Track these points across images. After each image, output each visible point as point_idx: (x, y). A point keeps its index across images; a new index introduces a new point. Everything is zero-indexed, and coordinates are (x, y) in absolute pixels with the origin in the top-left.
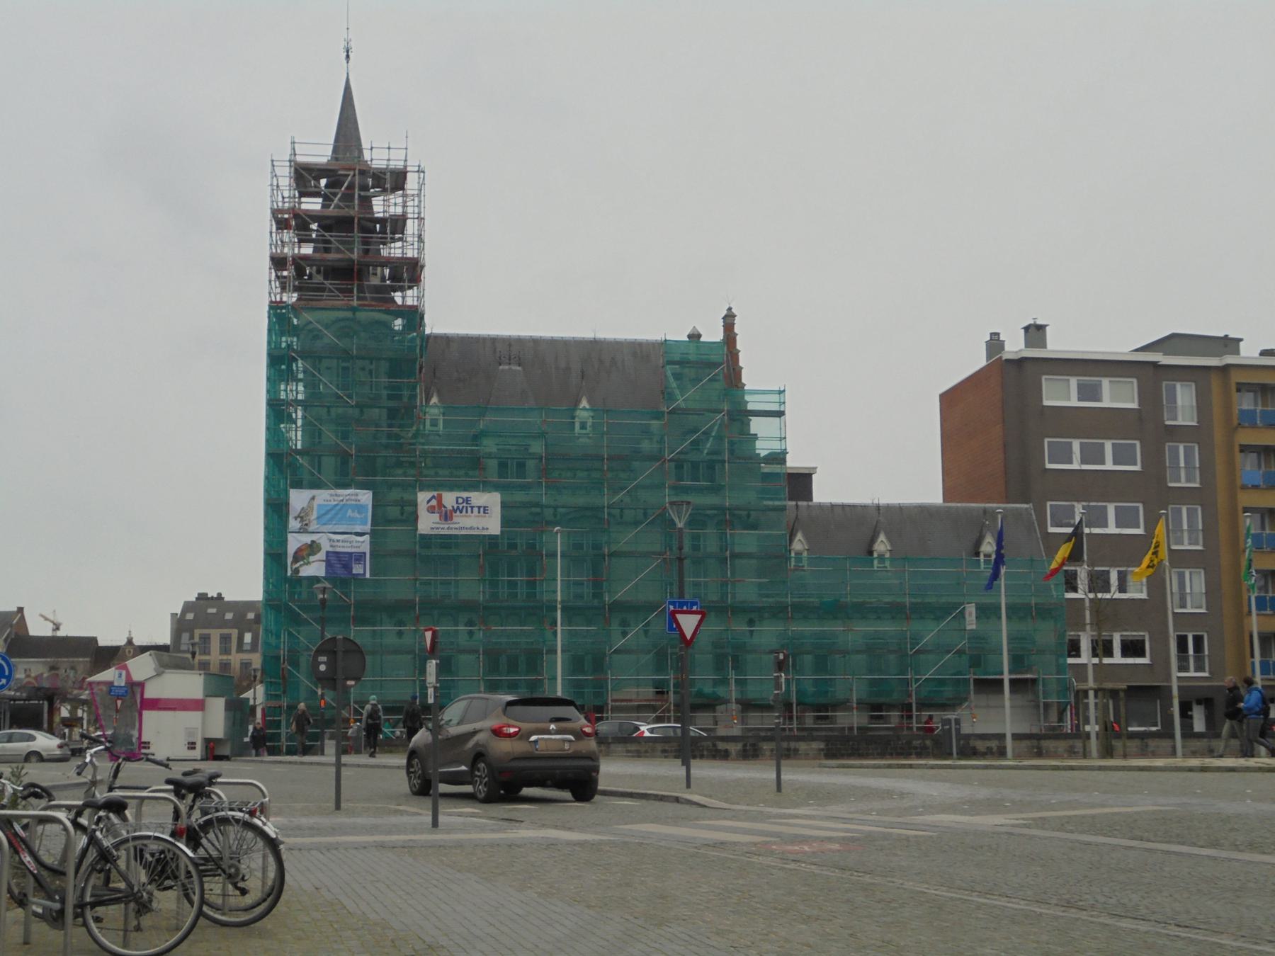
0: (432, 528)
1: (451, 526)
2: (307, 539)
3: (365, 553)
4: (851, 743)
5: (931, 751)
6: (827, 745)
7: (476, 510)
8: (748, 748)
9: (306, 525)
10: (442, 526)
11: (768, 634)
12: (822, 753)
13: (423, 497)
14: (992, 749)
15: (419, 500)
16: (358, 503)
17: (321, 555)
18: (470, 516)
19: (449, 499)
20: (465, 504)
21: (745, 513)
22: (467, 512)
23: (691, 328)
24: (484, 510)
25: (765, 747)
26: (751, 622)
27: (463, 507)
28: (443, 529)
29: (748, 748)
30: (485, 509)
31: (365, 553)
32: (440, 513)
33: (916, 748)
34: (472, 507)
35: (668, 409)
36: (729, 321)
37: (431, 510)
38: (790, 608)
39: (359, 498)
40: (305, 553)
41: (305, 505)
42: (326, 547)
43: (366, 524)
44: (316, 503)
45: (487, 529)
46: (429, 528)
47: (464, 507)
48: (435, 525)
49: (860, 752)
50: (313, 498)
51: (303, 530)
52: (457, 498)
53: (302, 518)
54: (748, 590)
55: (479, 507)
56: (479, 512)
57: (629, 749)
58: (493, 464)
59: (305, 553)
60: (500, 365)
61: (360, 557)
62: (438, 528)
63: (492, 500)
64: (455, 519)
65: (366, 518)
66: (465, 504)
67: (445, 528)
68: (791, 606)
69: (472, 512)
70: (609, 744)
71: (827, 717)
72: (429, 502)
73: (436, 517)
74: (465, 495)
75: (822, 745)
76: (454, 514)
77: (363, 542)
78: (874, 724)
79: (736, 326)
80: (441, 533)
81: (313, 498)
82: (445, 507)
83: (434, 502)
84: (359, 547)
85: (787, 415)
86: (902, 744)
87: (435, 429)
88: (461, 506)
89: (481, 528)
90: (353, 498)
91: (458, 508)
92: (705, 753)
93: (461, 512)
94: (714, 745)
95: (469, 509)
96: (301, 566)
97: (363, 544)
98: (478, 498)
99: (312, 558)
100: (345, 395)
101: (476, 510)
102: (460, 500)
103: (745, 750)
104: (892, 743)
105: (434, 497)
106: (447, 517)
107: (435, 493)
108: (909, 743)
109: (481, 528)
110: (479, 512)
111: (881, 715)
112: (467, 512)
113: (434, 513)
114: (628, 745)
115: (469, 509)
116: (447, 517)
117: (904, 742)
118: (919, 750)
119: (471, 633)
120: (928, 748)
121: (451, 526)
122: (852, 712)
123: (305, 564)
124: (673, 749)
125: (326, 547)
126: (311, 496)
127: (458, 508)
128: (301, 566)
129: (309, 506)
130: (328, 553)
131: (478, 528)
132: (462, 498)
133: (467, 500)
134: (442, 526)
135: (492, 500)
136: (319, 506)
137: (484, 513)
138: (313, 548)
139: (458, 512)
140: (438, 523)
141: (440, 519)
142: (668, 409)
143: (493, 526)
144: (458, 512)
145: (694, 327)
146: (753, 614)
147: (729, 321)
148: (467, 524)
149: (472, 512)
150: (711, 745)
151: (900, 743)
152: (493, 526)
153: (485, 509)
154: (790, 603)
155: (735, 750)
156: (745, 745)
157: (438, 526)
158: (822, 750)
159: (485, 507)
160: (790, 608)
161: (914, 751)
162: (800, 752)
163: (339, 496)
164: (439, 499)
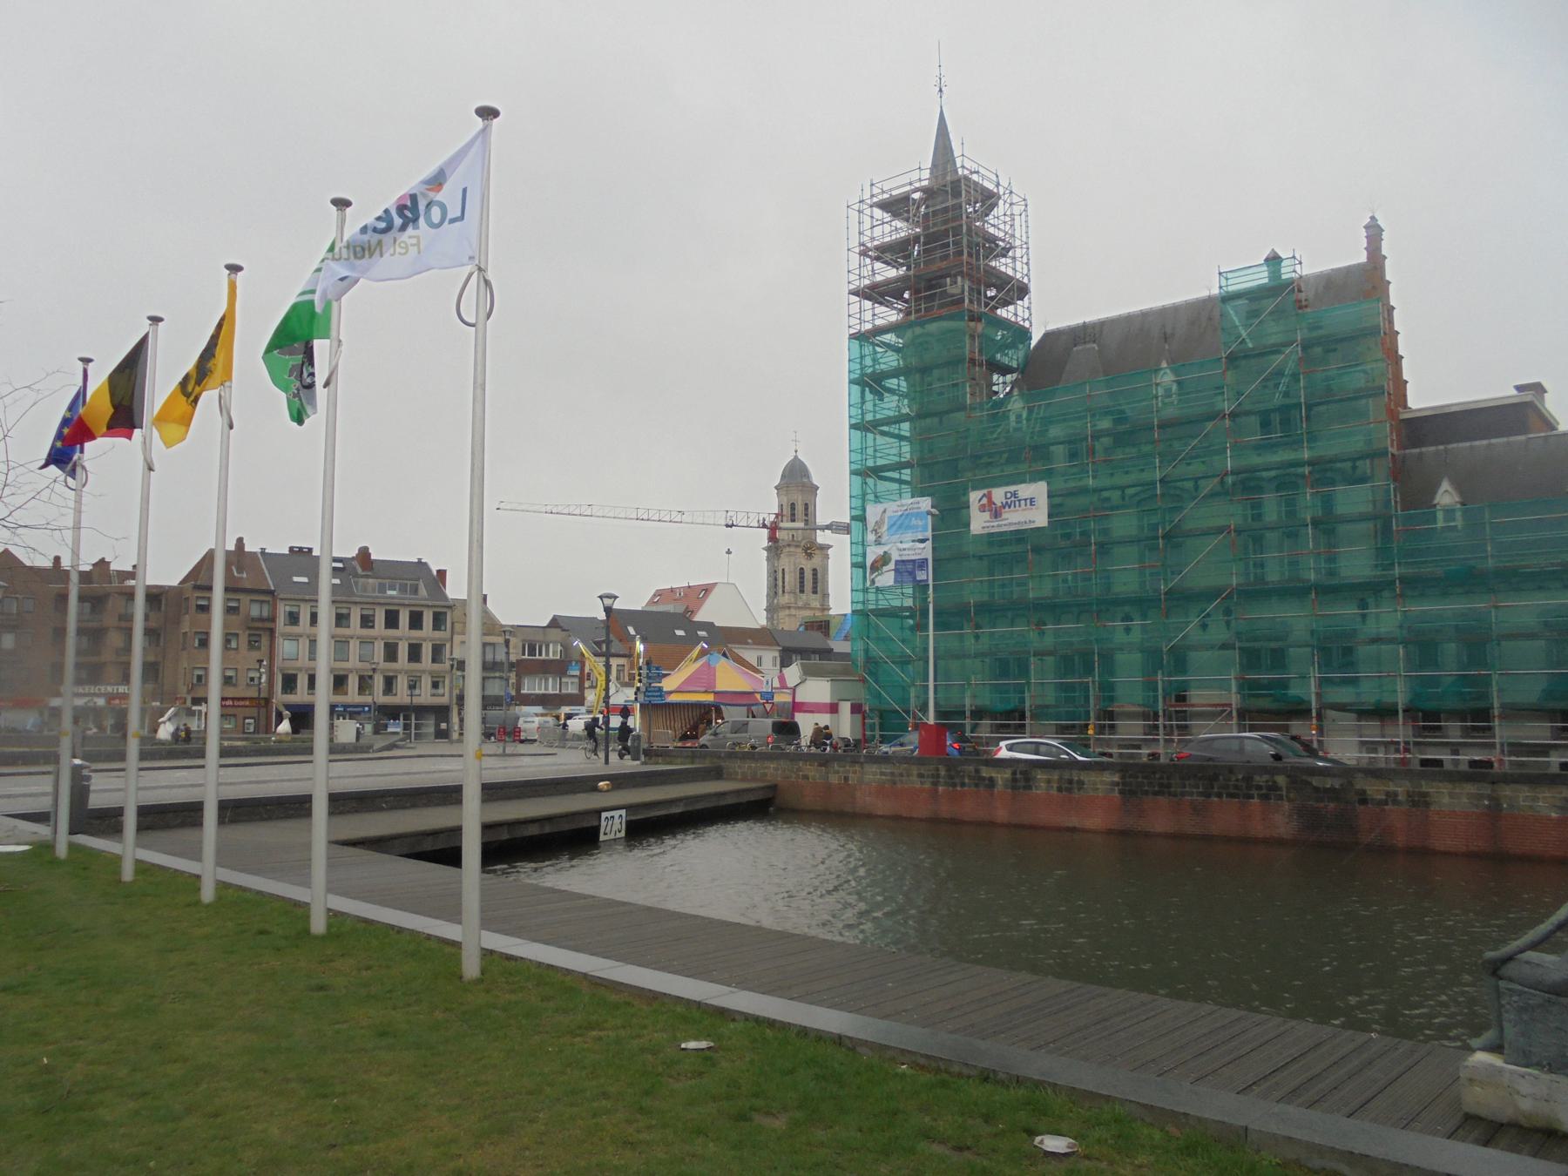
0: (984, 528)
1: (1000, 523)
2: (880, 551)
3: (927, 560)
4: (1157, 776)
5: (1284, 793)
6: (1123, 777)
7: (1023, 502)
8: (1018, 776)
9: (879, 537)
10: (992, 524)
11: (1387, 617)
12: (1116, 788)
13: (975, 497)
14: (1396, 794)
15: (971, 500)
16: (919, 510)
17: (892, 566)
18: (1018, 510)
19: (999, 495)
20: (1013, 499)
21: (1349, 464)
22: (1015, 506)
23: (1270, 250)
24: (1031, 502)
25: (1039, 777)
26: (1363, 605)
27: (1011, 502)
28: (993, 527)
29: (1018, 776)
30: (1032, 501)
31: (927, 560)
32: (990, 511)
33: (1259, 788)
34: (1019, 501)
35: (1225, 353)
36: (1374, 233)
37: (982, 509)
38: (1397, 582)
39: (920, 505)
40: (879, 565)
41: (878, 519)
42: (895, 556)
43: (926, 530)
44: (888, 514)
45: (1034, 522)
46: (980, 528)
47: (1013, 501)
48: (985, 525)
49: (1172, 790)
50: (885, 511)
51: (878, 543)
52: (1006, 493)
53: (876, 531)
54: (1357, 563)
55: (1026, 500)
56: (1026, 505)
57: (884, 770)
58: (1059, 451)
59: (879, 565)
60: (1075, 346)
61: (922, 564)
62: (988, 527)
63: (1038, 490)
64: (1004, 516)
65: (926, 525)
66: (1013, 499)
67: (998, 526)
68: (1399, 578)
69: (1020, 506)
70: (862, 763)
71: (1439, 728)
72: (980, 500)
73: (986, 516)
74: (1012, 488)
75: (1116, 778)
76: (1003, 510)
77: (924, 548)
78: (1430, 737)
79: (1384, 244)
80: (992, 531)
81: (885, 511)
82: (994, 504)
83: (985, 501)
84: (919, 554)
85: (1032, 293)
86: (1237, 780)
87: (1019, 425)
88: (1009, 501)
89: (1028, 521)
90: (916, 506)
91: (1007, 503)
92: (967, 781)
93: (1010, 507)
94: (977, 771)
95: (1017, 503)
96: (876, 576)
97: (926, 551)
98: (1025, 490)
99: (885, 568)
100: (998, 413)
101: (1023, 502)
102: (1009, 495)
103: (1014, 780)
104: (1221, 778)
105: (984, 495)
106: (996, 514)
107: (985, 491)
108: (1248, 779)
109: (1028, 521)
110: (1026, 505)
111: (1440, 726)
112: (1015, 506)
113: (984, 511)
114: (883, 766)
115: (1017, 503)
116: (996, 514)
117: (1240, 777)
118: (1264, 791)
119: (977, 637)
120: (1280, 789)
121: (1000, 523)
122: (1312, 721)
123: (879, 575)
124: (930, 773)
125: (895, 556)
126: (882, 509)
127: (1007, 503)
128: (876, 576)
129: (881, 519)
130: (897, 562)
131: (1026, 522)
132: (1011, 492)
133: (1014, 494)
134: (992, 524)
135: (1038, 490)
136: (889, 518)
137: (1031, 505)
138: (884, 560)
139: (1007, 507)
140: (989, 522)
141: (991, 518)
142: (1225, 353)
143: (1039, 517)
144: (1007, 507)
145: (1273, 250)
146: (1366, 592)
147: (1374, 233)
148: (1014, 519)
149: (1020, 506)
150: (973, 770)
151: (1234, 779)
152: (1039, 517)
153: (1032, 501)
154: (1397, 576)
155: (1001, 778)
156: (1014, 773)
157: (988, 524)
158: (1117, 784)
159: (1031, 499)
160: (1397, 582)
161: (1255, 792)
162: (1085, 786)
163: (903, 505)
164: (989, 496)
